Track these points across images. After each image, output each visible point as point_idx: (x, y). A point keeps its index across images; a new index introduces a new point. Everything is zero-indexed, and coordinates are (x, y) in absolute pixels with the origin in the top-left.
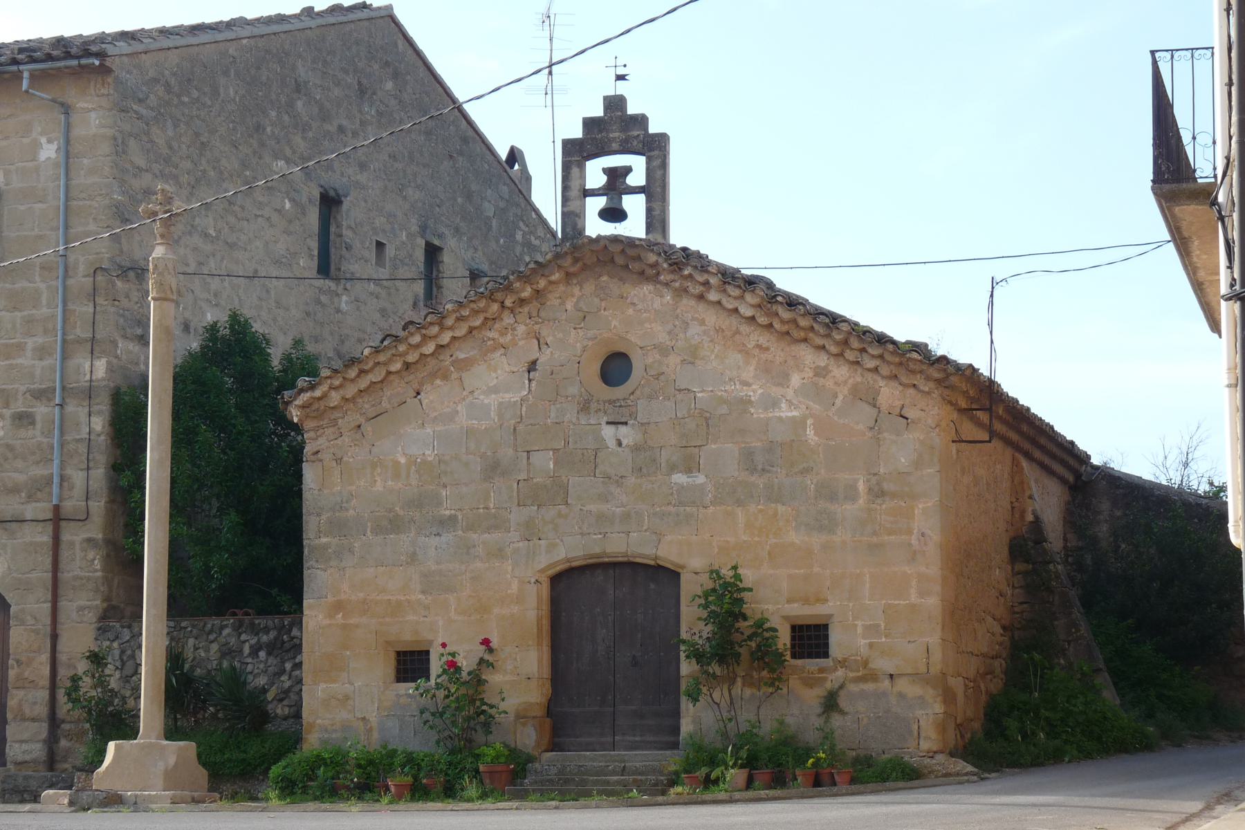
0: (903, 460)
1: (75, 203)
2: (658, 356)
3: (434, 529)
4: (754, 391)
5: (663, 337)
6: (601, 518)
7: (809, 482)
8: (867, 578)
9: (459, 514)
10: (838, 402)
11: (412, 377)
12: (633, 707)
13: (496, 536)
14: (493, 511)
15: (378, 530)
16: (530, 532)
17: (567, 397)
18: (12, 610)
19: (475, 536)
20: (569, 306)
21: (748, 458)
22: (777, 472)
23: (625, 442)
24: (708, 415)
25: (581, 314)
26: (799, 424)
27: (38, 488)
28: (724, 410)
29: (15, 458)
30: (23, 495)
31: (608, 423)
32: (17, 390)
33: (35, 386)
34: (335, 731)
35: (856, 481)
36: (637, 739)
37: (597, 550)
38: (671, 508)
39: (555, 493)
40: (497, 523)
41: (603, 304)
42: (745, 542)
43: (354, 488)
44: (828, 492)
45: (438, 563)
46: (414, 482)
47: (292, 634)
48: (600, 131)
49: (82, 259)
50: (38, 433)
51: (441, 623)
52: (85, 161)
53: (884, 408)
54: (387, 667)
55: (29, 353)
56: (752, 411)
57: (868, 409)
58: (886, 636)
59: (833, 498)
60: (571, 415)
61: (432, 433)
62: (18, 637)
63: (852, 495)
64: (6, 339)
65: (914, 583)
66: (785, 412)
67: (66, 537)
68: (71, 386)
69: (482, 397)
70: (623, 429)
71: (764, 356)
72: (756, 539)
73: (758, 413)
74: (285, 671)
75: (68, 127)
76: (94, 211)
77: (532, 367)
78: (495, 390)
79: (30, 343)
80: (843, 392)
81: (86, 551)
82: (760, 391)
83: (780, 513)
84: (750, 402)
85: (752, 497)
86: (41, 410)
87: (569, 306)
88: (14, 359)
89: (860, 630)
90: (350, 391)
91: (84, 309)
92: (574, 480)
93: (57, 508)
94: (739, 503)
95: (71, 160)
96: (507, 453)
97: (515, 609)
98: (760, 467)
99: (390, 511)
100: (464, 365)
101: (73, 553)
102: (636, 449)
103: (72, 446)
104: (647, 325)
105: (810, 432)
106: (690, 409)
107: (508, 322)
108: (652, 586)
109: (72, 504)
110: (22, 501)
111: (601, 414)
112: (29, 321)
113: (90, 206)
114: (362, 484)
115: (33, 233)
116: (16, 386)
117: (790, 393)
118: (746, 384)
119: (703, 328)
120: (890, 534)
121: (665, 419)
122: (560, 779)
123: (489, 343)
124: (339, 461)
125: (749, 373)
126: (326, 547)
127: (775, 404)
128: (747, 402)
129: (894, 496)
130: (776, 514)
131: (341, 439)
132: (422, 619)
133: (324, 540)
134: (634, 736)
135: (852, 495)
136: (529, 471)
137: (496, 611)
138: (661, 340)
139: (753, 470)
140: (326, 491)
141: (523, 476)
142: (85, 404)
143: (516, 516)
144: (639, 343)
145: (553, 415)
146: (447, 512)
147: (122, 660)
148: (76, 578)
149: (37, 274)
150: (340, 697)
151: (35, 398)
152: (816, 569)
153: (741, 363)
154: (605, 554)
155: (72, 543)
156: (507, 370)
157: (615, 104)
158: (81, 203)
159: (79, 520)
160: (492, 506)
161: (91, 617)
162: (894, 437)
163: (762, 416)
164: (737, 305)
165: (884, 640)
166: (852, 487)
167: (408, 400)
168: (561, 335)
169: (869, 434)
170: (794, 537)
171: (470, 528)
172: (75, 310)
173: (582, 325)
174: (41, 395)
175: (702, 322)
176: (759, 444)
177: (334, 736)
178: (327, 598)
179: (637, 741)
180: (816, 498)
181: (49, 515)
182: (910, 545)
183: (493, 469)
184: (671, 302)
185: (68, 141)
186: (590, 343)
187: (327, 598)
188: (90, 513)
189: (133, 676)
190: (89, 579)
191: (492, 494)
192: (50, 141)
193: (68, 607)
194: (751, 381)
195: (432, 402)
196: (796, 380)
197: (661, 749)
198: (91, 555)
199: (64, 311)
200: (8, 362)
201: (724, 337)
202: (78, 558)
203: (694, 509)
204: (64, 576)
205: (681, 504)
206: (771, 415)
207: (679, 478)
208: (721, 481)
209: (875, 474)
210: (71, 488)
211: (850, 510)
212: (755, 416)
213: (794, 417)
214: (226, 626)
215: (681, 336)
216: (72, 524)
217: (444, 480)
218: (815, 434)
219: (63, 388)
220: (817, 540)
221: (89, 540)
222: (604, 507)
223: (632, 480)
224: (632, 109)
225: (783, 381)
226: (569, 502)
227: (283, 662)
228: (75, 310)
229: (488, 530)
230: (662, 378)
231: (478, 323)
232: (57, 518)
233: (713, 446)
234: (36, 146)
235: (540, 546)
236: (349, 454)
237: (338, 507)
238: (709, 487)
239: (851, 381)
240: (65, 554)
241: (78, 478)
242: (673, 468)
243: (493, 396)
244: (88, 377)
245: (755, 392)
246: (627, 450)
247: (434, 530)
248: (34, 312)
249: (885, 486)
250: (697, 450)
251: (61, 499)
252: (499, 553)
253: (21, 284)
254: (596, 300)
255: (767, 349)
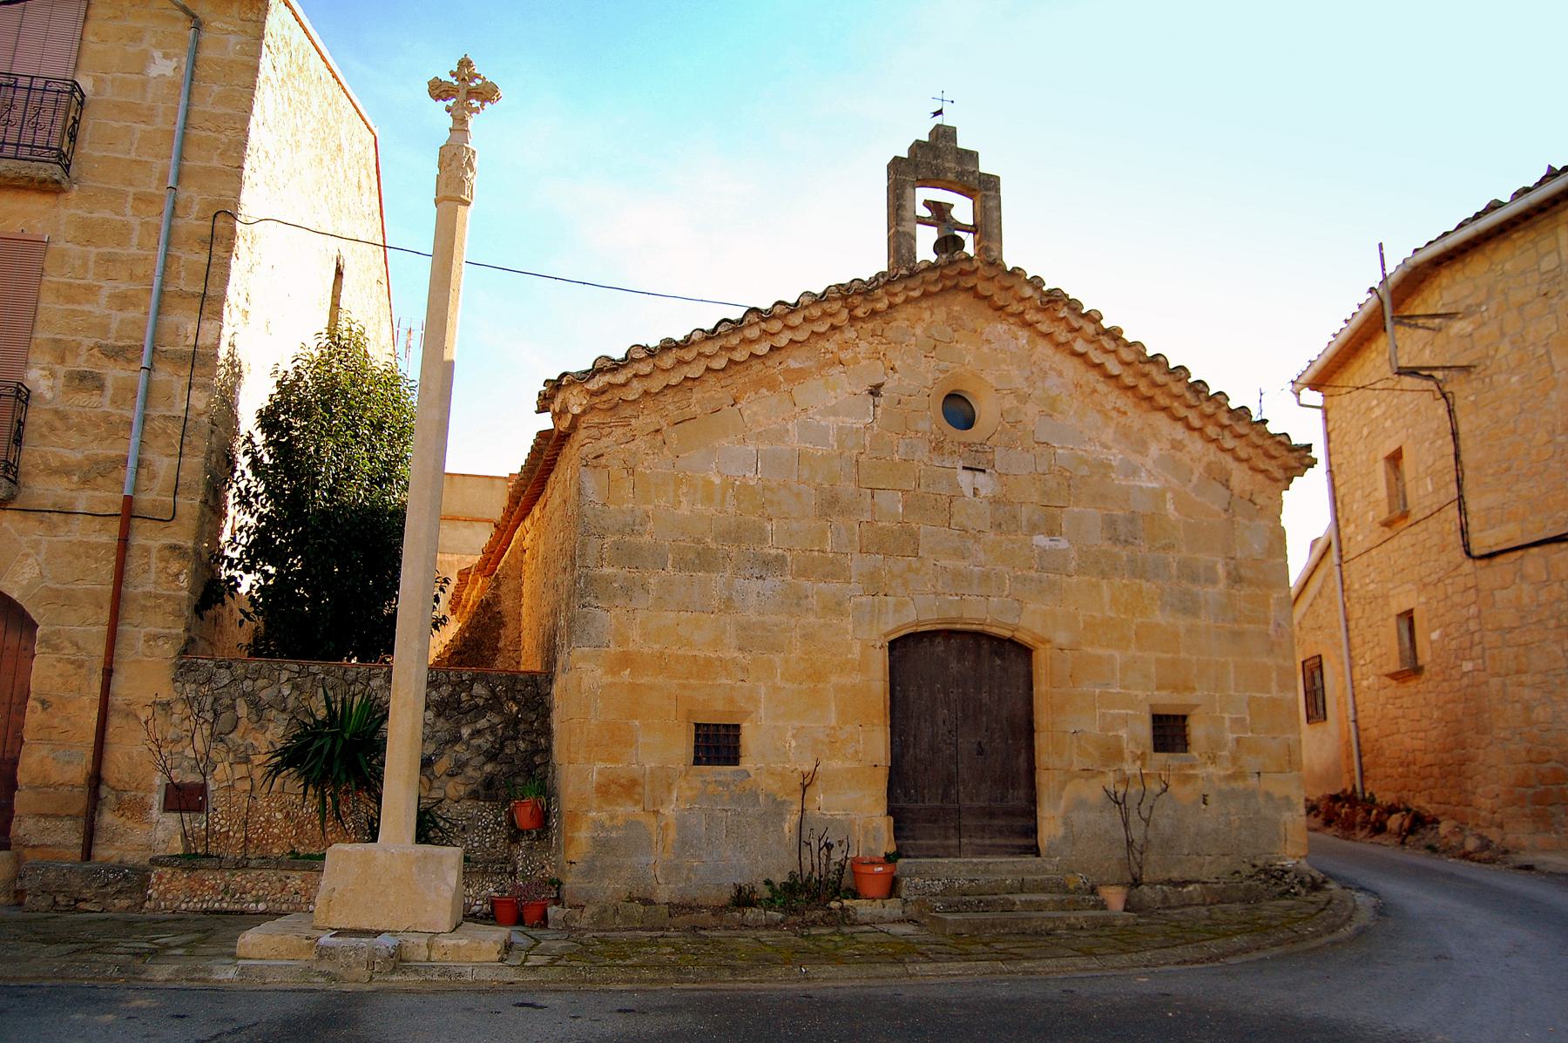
0: (1256, 547)
1: (195, 132)
2: (1015, 403)
3: (757, 571)
4: (1114, 455)
5: (1020, 383)
6: (957, 575)
7: (1171, 560)
8: (1231, 668)
9: (787, 554)
10: (1195, 479)
11: (729, 381)
12: (982, 804)
13: (835, 586)
14: (831, 555)
15: (681, 564)
16: (875, 586)
17: (917, 432)
18: (39, 633)
19: (808, 584)
20: (918, 331)
21: (1110, 523)
22: (1140, 545)
23: (983, 492)
24: (1068, 474)
25: (932, 342)
26: (1158, 496)
27: (96, 470)
28: (1085, 471)
29: (69, 428)
30: (75, 478)
31: (964, 468)
32: (79, 345)
33: (108, 342)
34: (617, 828)
35: (1215, 563)
36: (987, 842)
37: (954, 614)
38: (1033, 573)
39: (902, 542)
40: (834, 570)
41: (956, 335)
42: (1111, 618)
43: (651, 507)
44: (1190, 572)
45: (760, 614)
46: (731, 510)
47: (474, 692)
48: (936, 157)
49: (197, 199)
50: (107, 401)
51: (763, 690)
52: (215, 87)
53: (1237, 491)
54: (683, 746)
55: (103, 300)
56: (1114, 476)
57: (1223, 490)
58: (1252, 732)
59: (1194, 579)
60: (922, 454)
61: (755, 452)
62: (45, 671)
63: (1213, 581)
64: (71, 277)
65: (1274, 675)
66: (1146, 483)
67: (137, 540)
68: (164, 349)
69: (818, 417)
70: (979, 475)
71: (1123, 420)
72: (1123, 616)
73: (1118, 480)
74: (460, 738)
75: (197, 46)
76: (221, 146)
77: (875, 391)
78: (834, 411)
79: (107, 288)
80: (1198, 470)
81: (167, 562)
82: (1120, 456)
83: (1144, 589)
84: (1111, 466)
85: (1116, 569)
86: (114, 373)
87: (918, 331)
88: (79, 304)
89: (1227, 723)
90: (655, 385)
91: (195, 257)
92: (924, 529)
93: (128, 501)
94: (1103, 574)
95: (195, 83)
96: (847, 487)
97: (857, 679)
98: (1122, 538)
99: (699, 541)
100: (800, 375)
101: (147, 563)
102: (995, 501)
103: (157, 424)
104: (1003, 366)
105: (1170, 507)
106: (1050, 466)
107: (849, 335)
108: (998, 662)
109: (153, 496)
110: (73, 486)
111: (956, 457)
112: (110, 259)
113: (215, 139)
114: (663, 503)
115: (128, 157)
116: (78, 338)
117: (1150, 464)
118: (1104, 446)
119: (1061, 380)
120: (1248, 623)
121: (1024, 473)
122: (980, 902)
123: (828, 356)
124: (631, 471)
125: (1108, 435)
126: (609, 580)
127: (1133, 471)
128: (1106, 466)
129: (1251, 583)
130: (1140, 591)
131: (633, 443)
132: (739, 683)
133: (607, 570)
134: (983, 838)
135: (1213, 581)
136: (873, 513)
137: (834, 679)
138: (1018, 385)
139: (1115, 540)
140: (612, 507)
141: (866, 517)
142: (182, 373)
143: (858, 564)
144: (994, 385)
145: (901, 450)
146: (773, 552)
147: (215, 712)
148: (148, 595)
149: (129, 206)
150: (623, 781)
151: (106, 356)
152: (1183, 655)
153: (1099, 424)
154: (960, 619)
155: (146, 550)
156: (848, 390)
157: (944, 134)
158: (204, 134)
159: (162, 520)
160: (829, 550)
161: (169, 650)
162: (1247, 522)
163: (1123, 483)
164: (1103, 361)
165: (1250, 734)
166: (1211, 569)
167: (725, 407)
168: (910, 361)
169: (1224, 516)
170: (1160, 617)
171: (803, 573)
172: (179, 258)
173: (933, 354)
174: (114, 354)
175: (1060, 374)
176: (1120, 513)
177: (614, 835)
178: (608, 647)
179: (984, 846)
180: (1178, 577)
181: (116, 509)
182: (1268, 635)
183: (831, 504)
184: (1026, 346)
185: (194, 63)
186: (942, 376)
187: (608, 647)
188: (178, 512)
189: (230, 732)
190: (169, 598)
191: (829, 535)
192: (166, 56)
193: (135, 631)
194: (1110, 444)
195: (755, 414)
196: (1154, 450)
197: (1013, 854)
198: (174, 567)
199: (167, 255)
200: (70, 306)
201: (1082, 393)
202: (153, 570)
203: (1058, 577)
204: (129, 590)
205: (1043, 569)
206: (1132, 483)
207: (1041, 540)
208: (1085, 549)
209: (1232, 558)
210: (153, 477)
211: (1213, 593)
212: (1116, 482)
213: (1153, 488)
214: (376, 676)
215: (1039, 384)
216: (149, 523)
217: (769, 511)
218: (1176, 509)
219: (154, 350)
220: (1182, 622)
221: (173, 548)
222: (961, 564)
223: (991, 536)
224: (963, 143)
225: (1141, 447)
226: (920, 554)
227: (458, 724)
228: (179, 258)
229: (825, 577)
230: (1019, 426)
231: (823, 329)
232: (128, 513)
233: (1075, 509)
234: (145, 59)
235: (886, 602)
236: (646, 464)
237: (628, 530)
238: (1073, 554)
239: (1205, 459)
240: (134, 564)
241: (163, 465)
242: (1034, 529)
243: (832, 418)
244: (192, 341)
245: (1116, 456)
246: (985, 501)
247: (756, 572)
248: (117, 250)
249: (1243, 572)
250: (1059, 511)
251: (136, 489)
252: (836, 607)
253: (102, 214)
254: (949, 330)
255: (1125, 413)
